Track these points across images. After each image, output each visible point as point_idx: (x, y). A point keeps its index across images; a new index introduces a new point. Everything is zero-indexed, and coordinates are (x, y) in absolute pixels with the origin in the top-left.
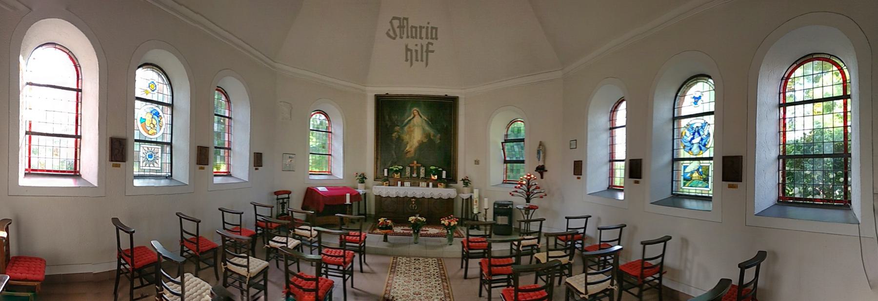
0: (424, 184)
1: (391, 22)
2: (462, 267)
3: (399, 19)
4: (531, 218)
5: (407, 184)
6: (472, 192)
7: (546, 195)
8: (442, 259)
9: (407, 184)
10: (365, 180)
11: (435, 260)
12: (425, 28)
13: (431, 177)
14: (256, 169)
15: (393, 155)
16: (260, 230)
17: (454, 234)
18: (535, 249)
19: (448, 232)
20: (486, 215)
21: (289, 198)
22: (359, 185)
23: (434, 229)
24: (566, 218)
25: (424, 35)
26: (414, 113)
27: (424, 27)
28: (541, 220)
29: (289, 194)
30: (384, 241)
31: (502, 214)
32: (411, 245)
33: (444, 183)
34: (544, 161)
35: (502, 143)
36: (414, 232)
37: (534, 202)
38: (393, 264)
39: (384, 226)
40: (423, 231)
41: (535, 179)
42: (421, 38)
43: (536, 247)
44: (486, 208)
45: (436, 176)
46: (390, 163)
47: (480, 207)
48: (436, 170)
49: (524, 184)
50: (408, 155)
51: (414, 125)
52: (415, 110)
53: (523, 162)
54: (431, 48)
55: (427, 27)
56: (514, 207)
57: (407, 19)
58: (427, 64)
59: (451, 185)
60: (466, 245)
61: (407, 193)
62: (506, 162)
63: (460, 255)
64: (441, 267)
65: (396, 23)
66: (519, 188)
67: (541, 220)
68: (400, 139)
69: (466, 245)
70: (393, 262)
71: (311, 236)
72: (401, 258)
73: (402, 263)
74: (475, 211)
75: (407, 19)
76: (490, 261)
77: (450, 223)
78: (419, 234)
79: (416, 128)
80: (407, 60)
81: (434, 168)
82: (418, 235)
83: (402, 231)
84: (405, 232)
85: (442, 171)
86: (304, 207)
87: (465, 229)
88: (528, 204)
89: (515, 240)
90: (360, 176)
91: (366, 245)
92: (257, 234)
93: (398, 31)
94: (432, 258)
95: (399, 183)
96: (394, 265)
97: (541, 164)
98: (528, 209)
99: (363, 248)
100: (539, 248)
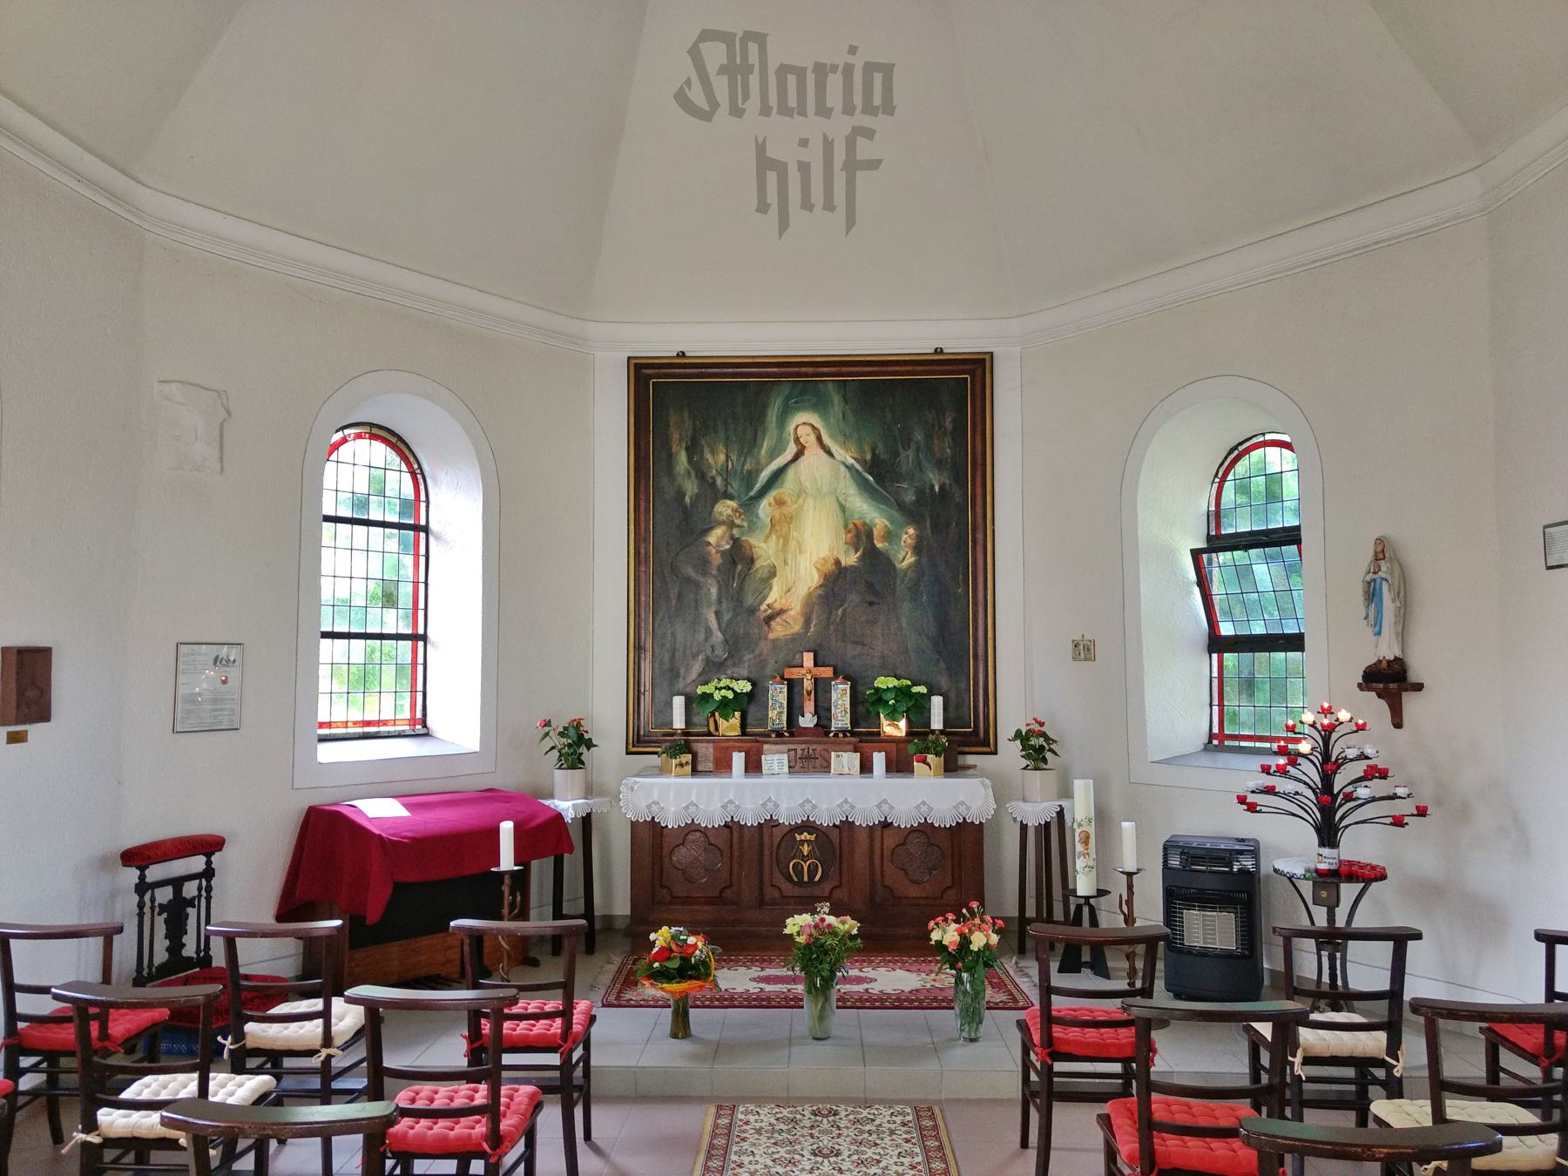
0: (846, 761)
1: (695, 54)
2: (1024, 1144)
3: (726, 38)
4: (1349, 921)
5: (775, 760)
6: (1066, 793)
7: (1422, 812)
8: (937, 1110)
9: (775, 760)
10: (586, 755)
11: (903, 1114)
12: (840, 69)
13: (879, 725)
14: (15, 738)
15: (709, 631)
16: (34, 1069)
17: (989, 992)
18: (1376, 1081)
19: (959, 980)
20: (1130, 902)
21: (209, 873)
22: (562, 778)
23: (900, 973)
24: (1539, 936)
25: (834, 98)
26: (797, 440)
27: (834, 68)
28: (1401, 939)
29: (209, 855)
30: (674, 1036)
31: (1207, 900)
32: (796, 1050)
33: (937, 754)
34: (1403, 636)
35: (1196, 554)
36: (811, 988)
37: (1358, 845)
38: (714, 1135)
39: (674, 964)
40: (846, 980)
41: (1361, 728)
42: (824, 111)
43: (1380, 1073)
44: (1131, 868)
45: (903, 724)
46: (697, 667)
47: (1103, 865)
48: (902, 693)
49: (1305, 756)
50: (778, 630)
51: (800, 493)
52: (804, 422)
53: (1294, 642)
54: (865, 149)
55: (848, 70)
56: (1265, 869)
57: (761, 39)
58: (851, 222)
59: (971, 760)
60: (1036, 1038)
61: (776, 806)
62: (1217, 644)
63: (1014, 1089)
64: (932, 1143)
65: (715, 55)
66: (1282, 771)
67: (1401, 939)
68: (739, 557)
69: (1036, 1038)
70: (716, 1126)
71: (328, 1039)
72: (751, 1107)
73: (759, 1131)
74: (1084, 885)
75: (761, 39)
76: (1145, 1104)
77: (965, 941)
78: (834, 997)
79: (810, 500)
80: (763, 207)
81: (892, 682)
82: (827, 999)
83: (753, 988)
84: (769, 988)
85: (928, 697)
86: (293, 906)
87: (1033, 968)
88: (1326, 851)
89: (1261, 1017)
90: (561, 734)
91: (595, 1061)
92: (16, 1093)
93: (721, 85)
94: (889, 1103)
95: (738, 759)
96: (720, 1141)
97: (1387, 649)
98: (1328, 881)
99: (579, 1072)
100: (1400, 1080)
